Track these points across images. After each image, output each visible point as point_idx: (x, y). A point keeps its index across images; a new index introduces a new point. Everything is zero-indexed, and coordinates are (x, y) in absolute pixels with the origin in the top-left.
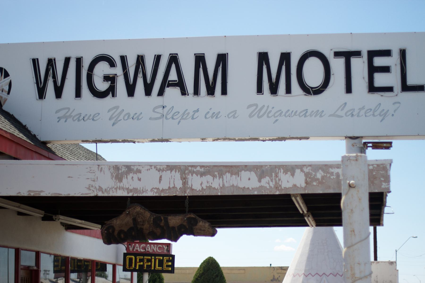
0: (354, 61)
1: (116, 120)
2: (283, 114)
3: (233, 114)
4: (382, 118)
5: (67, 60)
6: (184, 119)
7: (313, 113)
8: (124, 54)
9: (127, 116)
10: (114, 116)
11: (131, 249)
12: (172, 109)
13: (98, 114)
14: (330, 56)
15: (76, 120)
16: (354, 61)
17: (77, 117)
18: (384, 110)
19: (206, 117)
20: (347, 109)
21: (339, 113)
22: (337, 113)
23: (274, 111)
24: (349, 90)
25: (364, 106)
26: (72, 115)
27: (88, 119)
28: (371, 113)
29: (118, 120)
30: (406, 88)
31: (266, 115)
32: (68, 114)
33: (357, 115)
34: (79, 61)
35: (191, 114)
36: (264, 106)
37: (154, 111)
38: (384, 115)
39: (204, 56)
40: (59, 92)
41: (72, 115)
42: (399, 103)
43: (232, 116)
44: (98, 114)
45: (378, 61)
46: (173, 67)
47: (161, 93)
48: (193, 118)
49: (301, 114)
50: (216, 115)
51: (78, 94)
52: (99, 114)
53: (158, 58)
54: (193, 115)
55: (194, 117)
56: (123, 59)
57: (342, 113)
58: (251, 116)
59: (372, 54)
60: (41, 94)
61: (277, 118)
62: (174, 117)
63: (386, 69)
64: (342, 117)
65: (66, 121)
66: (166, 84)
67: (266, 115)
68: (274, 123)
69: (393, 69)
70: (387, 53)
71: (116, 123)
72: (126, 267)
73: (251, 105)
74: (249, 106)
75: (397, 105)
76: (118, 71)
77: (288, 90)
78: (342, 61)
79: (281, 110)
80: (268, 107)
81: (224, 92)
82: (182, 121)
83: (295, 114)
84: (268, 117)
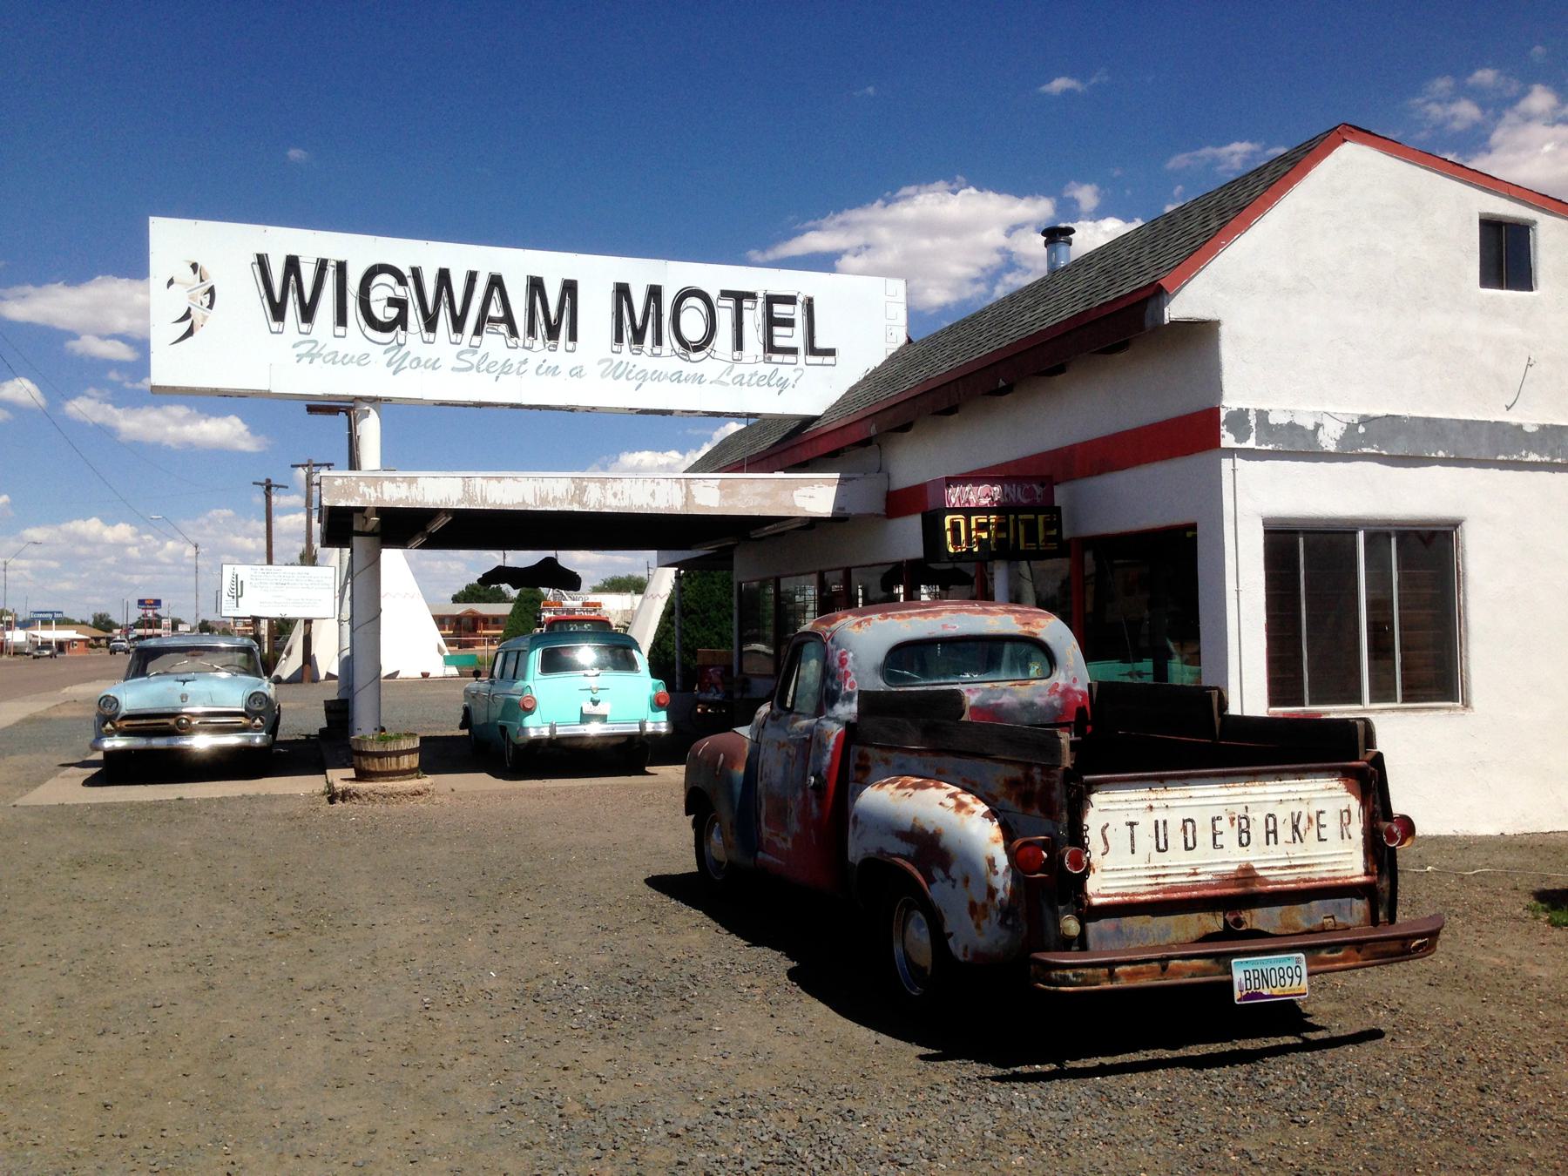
0: (747, 304)
2: (649, 375)
4: (780, 388)
5: (322, 265)
6: (506, 373)
8: (416, 265)
10: (639, 322)
14: (714, 295)
16: (747, 304)
17: (332, 356)
21: (725, 378)
22: (721, 379)
23: (636, 371)
28: (766, 380)
30: (812, 350)
31: (624, 377)
32: (315, 351)
34: (341, 268)
35: (516, 366)
37: (458, 357)
38: (783, 385)
40: (308, 313)
45: (780, 310)
47: (478, 331)
51: (342, 319)
52: (368, 355)
56: (416, 273)
57: (728, 379)
59: (771, 300)
60: (278, 312)
62: (491, 370)
63: (789, 323)
67: (624, 377)
70: (790, 300)
74: (600, 363)
76: (408, 293)
78: (730, 303)
81: (573, 336)
82: (501, 376)
83: (351, 361)
84: (628, 379)
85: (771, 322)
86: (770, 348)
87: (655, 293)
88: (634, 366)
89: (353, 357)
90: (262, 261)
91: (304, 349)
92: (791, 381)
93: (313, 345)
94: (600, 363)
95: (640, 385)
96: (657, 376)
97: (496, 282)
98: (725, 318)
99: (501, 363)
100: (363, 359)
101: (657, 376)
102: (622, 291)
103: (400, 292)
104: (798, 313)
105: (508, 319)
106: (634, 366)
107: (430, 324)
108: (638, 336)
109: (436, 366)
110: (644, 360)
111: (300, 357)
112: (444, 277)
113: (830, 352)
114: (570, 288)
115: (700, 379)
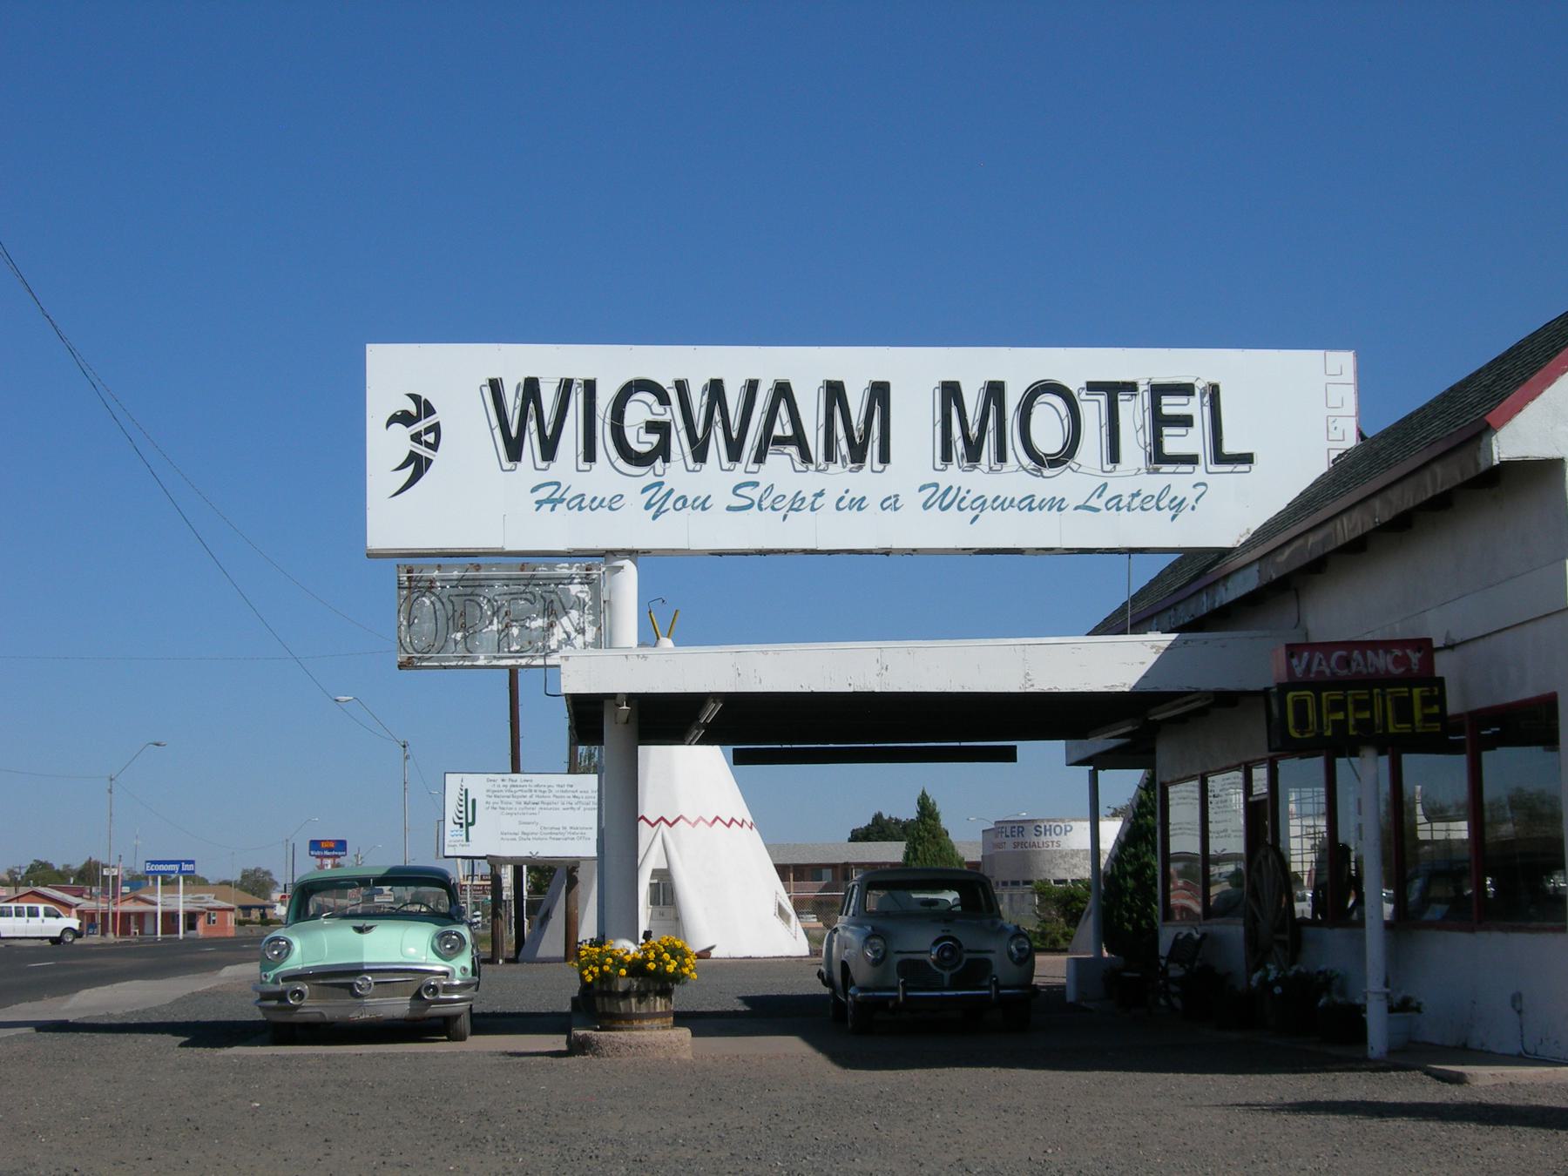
0: (1166, 411)
1: (658, 511)
3: (891, 503)
5: (566, 386)
6: (797, 510)
7: (855, 501)
8: (681, 377)
9: (681, 501)
10: (653, 502)
11: (1299, 671)
12: (1102, 492)
13: (619, 497)
15: (573, 507)
16: (1166, 411)
18: (1175, 498)
19: (838, 508)
20: (1107, 495)
21: (1094, 503)
23: (970, 498)
24: (1114, 457)
25: (823, 490)
26: (564, 497)
27: (600, 505)
29: (662, 510)
30: (1220, 458)
32: (557, 496)
33: (810, 507)
34: (590, 387)
35: (809, 500)
36: (951, 488)
37: (734, 492)
38: (1178, 506)
39: (750, 381)
40: (549, 449)
41: (564, 497)
42: (1205, 484)
43: (998, 506)
44: (619, 497)
45: (1171, 405)
46: (783, 409)
47: (760, 458)
48: (813, 509)
49: (1022, 506)
50: (859, 504)
51: (590, 456)
52: (622, 496)
53: (752, 386)
54: (813, 503)
55: (816, 507)
56: (681, 386)
58: (926, 506)
59: (1158, 391)
60: (514, 450)
61: (977, 512)
63: (1186, 421)
64: (1098, 510)
65: (553, 509)
66: (768, 441)
68: (972, 523)
69: (1197, 421)
71: (658, 516)
72: (1312, 694)
73: (925, 485)
74: (922, 488)
75: (1202, 488)
76: (673, 414)
77: (1001, 457)
79: (982, 497)
80: (959, 489)
81: (885, 457)
85: (1160, 421)
86: (1158, 457)
87: (995, 391)
88: (968, 492)
89: (603, 500)
90: (495, 386)
91: (544, 493)
92: (1190, 501)
93: (556, 487)
94: (922, 488)
95: (977, 517)
96: (1001, 504)
97: (783, 391)
98: (1093, 411)
99: (790, 497)
100: (613, 503)
101: (1001, 504)
102: (951, 392)
103: (661, 414)
104: (1194, 406)
105: (798, 439)
106: (968, 492)
107: (700, 453)
108: (973, 452)
109: (707, 506)
110: (980, 480)
111: (540, 503)
112: (716, 389)
113: (1247, 459)
114: (880, 393)
115: (1057, 505)
